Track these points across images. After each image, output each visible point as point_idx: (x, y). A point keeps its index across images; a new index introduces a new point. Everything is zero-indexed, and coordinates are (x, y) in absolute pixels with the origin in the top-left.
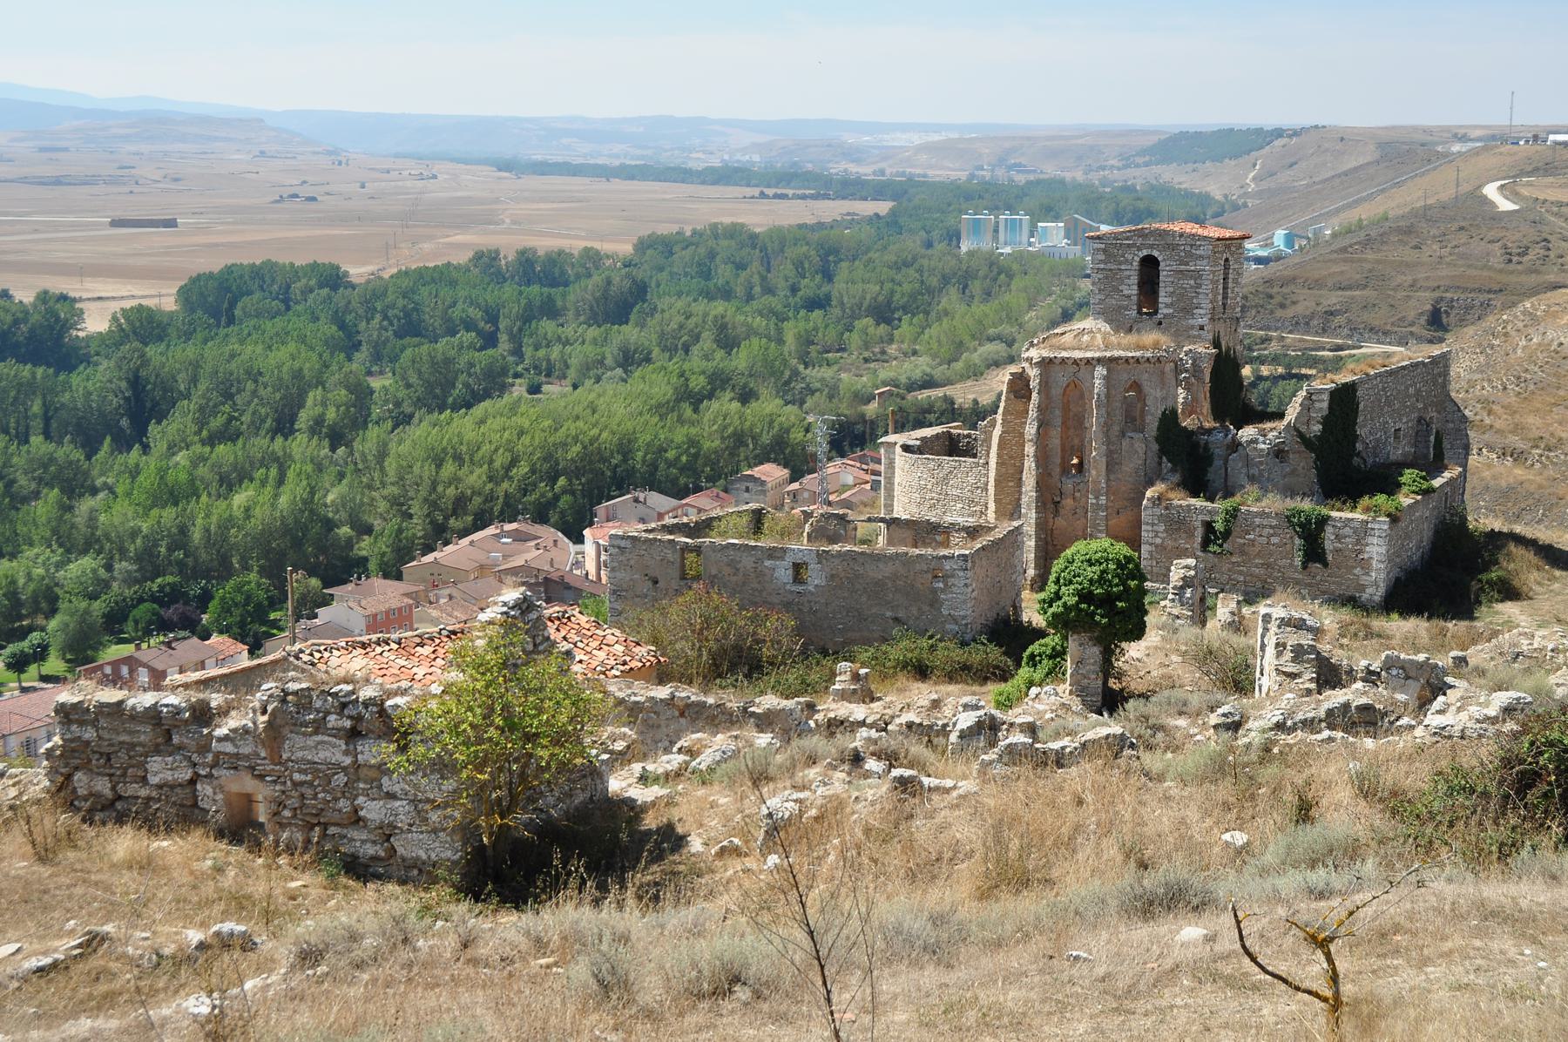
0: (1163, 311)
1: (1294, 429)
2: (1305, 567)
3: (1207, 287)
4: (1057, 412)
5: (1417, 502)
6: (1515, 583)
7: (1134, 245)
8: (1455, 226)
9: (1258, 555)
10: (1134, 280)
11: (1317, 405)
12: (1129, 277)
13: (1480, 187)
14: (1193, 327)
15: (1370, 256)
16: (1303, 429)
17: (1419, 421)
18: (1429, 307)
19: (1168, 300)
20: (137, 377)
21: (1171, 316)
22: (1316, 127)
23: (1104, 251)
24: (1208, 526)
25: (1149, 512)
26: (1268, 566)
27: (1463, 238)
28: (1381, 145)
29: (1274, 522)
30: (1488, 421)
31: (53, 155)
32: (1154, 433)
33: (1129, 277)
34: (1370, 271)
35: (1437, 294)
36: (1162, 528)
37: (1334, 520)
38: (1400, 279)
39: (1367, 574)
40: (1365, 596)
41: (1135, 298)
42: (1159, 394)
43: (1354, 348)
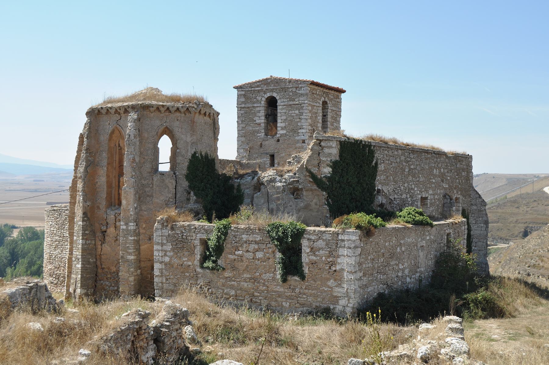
0: (280, 132)
1: (306, 170)
2: (284, 280)
3: (307, 114)
4: (105, 155)
5: (405, 228)
6: (501, 304)
8: (533, 200)
9: (246, 270)
11: (326, 150)
13: (543, 188)
14: (298, 141)
15: (500, 211)
16: (315, 170)
17: (445, 196)
18: (523, 230)
19: (283, 125)
20: (13, 251)
21: (285, 135)
22: (485, 173)
23: (244, 95)
24: (205, 243)
25: (159, 233)
26: (254, 280)
27: (535, 204)
28: (507, 179)
29: (258, 238)
30: (541, 264)
31: (37, 183)
32: (185, 172)
33: (282, 109)
34: (500, 216)
35: (526, 225)
36: (169, 247)
37: (309, 233)
38: (511, 219)
39: (339, 286)
40: (339, 308)
41: (263, 125)
42: (189, 139)
43: (494, 245)
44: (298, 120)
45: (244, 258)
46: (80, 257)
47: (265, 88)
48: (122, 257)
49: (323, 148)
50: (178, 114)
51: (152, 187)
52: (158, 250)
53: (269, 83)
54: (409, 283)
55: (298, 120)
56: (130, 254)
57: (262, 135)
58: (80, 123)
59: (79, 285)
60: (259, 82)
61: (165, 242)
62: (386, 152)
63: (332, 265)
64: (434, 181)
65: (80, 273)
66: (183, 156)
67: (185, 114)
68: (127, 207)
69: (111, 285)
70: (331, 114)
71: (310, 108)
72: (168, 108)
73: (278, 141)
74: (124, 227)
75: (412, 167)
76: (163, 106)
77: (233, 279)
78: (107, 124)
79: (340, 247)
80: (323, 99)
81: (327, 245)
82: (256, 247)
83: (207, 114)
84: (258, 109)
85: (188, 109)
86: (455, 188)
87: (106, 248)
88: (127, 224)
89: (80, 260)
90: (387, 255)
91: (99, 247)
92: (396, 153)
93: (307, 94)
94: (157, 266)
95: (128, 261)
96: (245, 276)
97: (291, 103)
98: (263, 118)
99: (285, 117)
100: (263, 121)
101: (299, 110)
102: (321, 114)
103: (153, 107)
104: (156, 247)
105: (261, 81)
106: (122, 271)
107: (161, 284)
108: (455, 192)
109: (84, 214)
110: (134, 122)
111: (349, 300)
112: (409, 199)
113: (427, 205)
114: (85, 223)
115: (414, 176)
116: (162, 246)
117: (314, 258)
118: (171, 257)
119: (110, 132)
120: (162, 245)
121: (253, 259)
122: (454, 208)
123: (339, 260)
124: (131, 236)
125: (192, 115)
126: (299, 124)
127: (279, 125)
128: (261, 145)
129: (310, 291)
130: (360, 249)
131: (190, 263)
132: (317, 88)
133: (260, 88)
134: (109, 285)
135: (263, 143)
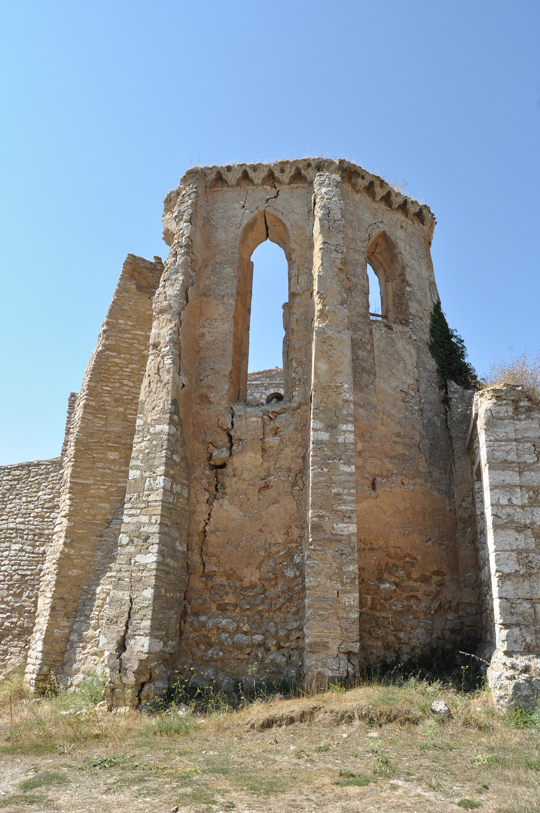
46: (155, 529)
47: (267, 381)
48: (316, 527)
53: (274, 376)
56: (345, 517)
59: (147, 623)
60: (258, 373)
65: (153, 581)
66: (419, 302)
69: (238, 630)
74: (324, 436)
78: (238, 206)
87: (227, 511)
88: (331, 427)
89: (155, 539)
91: (203, 508)
95: (337, 539)
103: (363, 178)
105: (262, 373)
106: (318, 573)
107: (527, 605)
109: (174, 402)
110: (337, 187)
116: (520, 473)
119: (245, 222)
124: (348, 463)
133: (259, 382)
134: (232, 627)
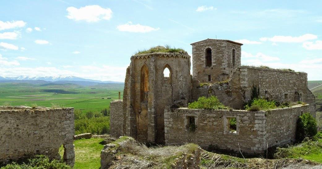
0: (213, 64)
7: (204, 45)
10: (204, 56)
11: (243, 73)
12: (203, 55)
14: (222, 69)
17: (296, 93)
19: (214, 61)
21: (216, 66)
23: (196, 48)
33: (203, 55)
41: (205, 61)
44: (222, 59)
45: (208, 125)
49: (241, 72)
50: (172, 58)
51: (162, 92)
52: (167, 121)
54: (286, 136)
55: (222, 59)
56: (152, 123)
57: (204, 66)
58: (128, 63)
61: (169, 117)
62: (269, 73)
63: (252, 128)
64: (290, 86)
67: (176, 58)
68: (151, 101)
70: (237, 56)
71: (227, 53)
72: (168, 55)
73: (212, 68)
75: (281, 80)
76: (165, 54)
77: (203, 134)
79: (256, 119)
80: (233, 48)
81: (249, 118)
82: (214, 119)
83: (186, 57)
84: (202, 54)
85: (177, 55)
86: (300, 89)
88: (151, 109)
90: (276, 123)
92: (273, 73)
93: (225, 47)
94: (166, 128)
95: (152, 126)
96: (208, 133)
97: (218, 51)
98: (205, 58)
99: (215, 58)
100: (204, 60)
101: (222, 54)
102: (232, 56)
103: (161, 55)
104: (165, 120)
108: (300, 91)
111: (260, 145)
112: (279, 95)
113: (287, 97)
114: (131, 109)
115: (281, 84)
117: (243, 125)
118: (172, 125)
120: (168, 119)
121: (212, 125)
122: (300, 99)
123: (255, 126)
124: (153, 115)
125: (179, 58)
126: (222, 61)
127: (212, 61)
128: (204, 71)
129: (241, 140)
130: (265, 120)
131: (182, 127)
132: (230, 43)
135: (205, 70)
